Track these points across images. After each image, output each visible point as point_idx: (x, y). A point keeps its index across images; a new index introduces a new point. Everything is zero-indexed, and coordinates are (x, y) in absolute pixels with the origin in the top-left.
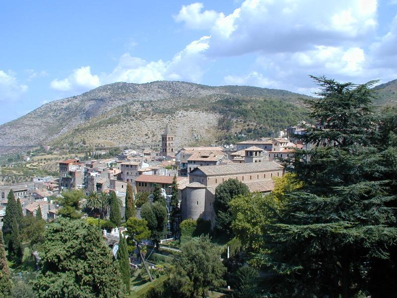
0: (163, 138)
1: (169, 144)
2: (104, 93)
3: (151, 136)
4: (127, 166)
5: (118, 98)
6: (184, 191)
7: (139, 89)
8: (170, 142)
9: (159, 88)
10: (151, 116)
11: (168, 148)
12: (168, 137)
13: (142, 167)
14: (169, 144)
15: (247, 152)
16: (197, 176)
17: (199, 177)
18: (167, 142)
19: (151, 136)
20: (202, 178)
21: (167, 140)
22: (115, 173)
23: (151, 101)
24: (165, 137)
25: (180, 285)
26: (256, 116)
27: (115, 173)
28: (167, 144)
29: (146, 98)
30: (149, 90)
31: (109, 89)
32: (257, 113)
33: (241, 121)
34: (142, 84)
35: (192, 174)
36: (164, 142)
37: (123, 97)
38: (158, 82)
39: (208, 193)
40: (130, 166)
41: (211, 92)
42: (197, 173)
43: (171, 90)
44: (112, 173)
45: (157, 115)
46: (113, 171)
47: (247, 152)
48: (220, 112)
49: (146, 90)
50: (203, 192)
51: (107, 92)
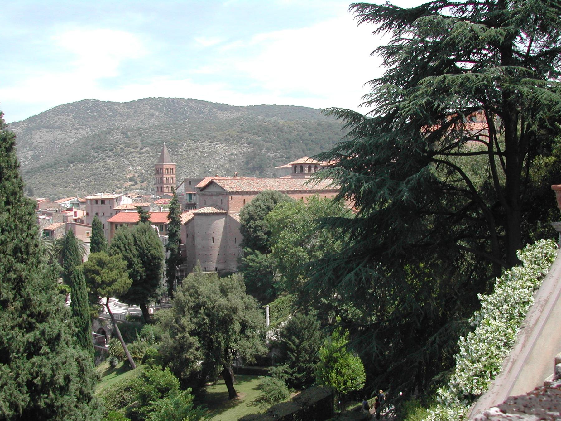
0: (157, 170)
1: (167, 179)
2: (63, 118)
3: (138, 180)
4: (97, 201)
5: (86, 125)
6: (190, 224)
7: (120, 110)
8: (169, 176)
9: (151, 109)
10: (138, 149)
11: (165, 186)
12: (165, 167)
13: (122, 203)
14: (167, 179)
15: (295, 166)
16: (211, 195)
17: (215, 198)
18: (165, 176)
19: (138, 180)
20: (221, 197)
21: (164, 172)
22: (76, 216)
23: (139, 129)
24: (160, 167)
25: (167, 281)
26: (305, 147)
27: (76, 216)
28: (165, 179)
29: (130, 123)
30: (135, 112)
31: (72, 111)
32: (306, 144)
33: (282, 157)
34: (125, 103)
35: (203, 192)
36: (158, 176)
37: (95, 123)
38: (150, 99)
39: (230, 221)
40: (100, 202)
41: (236, 115)
42: (211, 189)
43: (170, 111)
44: (72, 216)
45: (148, 148)
46: (72, 213)
47: (295, 167)
48: (249, 143)
49: (132, 112)
50: (221, 222)
51: (68, 116)
